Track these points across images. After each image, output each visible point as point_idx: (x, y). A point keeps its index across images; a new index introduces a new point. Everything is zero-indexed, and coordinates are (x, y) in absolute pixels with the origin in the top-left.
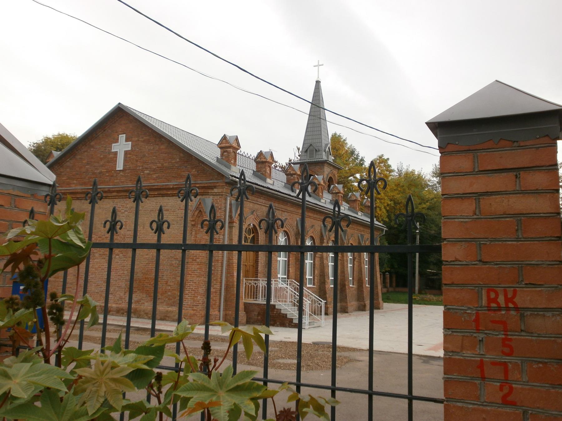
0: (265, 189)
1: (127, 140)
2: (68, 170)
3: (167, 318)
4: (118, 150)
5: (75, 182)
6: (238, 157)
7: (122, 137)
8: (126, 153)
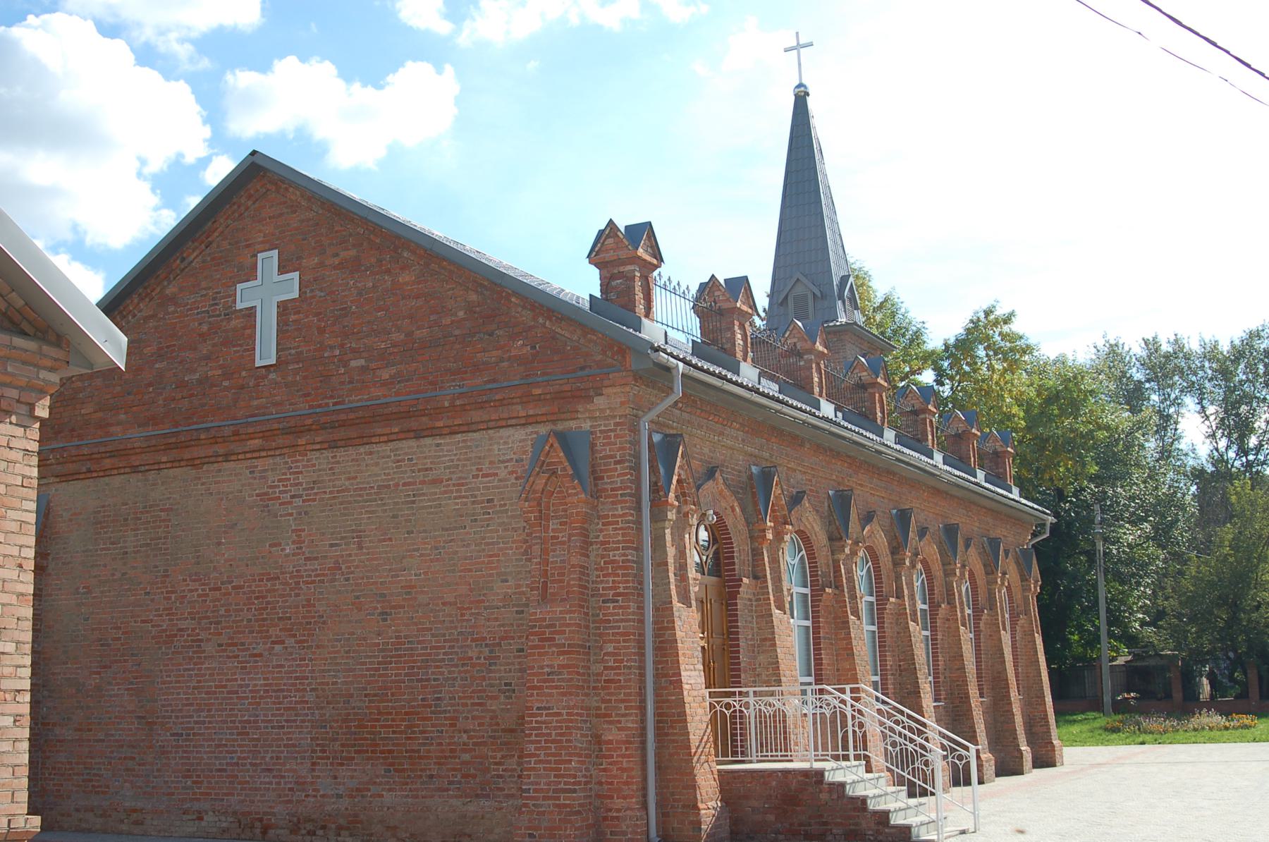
1: (283, 269)
4: (257, 303)
5: (123, 416)
6: (658, 296)
7: (269, 260)
8: (283, 307)
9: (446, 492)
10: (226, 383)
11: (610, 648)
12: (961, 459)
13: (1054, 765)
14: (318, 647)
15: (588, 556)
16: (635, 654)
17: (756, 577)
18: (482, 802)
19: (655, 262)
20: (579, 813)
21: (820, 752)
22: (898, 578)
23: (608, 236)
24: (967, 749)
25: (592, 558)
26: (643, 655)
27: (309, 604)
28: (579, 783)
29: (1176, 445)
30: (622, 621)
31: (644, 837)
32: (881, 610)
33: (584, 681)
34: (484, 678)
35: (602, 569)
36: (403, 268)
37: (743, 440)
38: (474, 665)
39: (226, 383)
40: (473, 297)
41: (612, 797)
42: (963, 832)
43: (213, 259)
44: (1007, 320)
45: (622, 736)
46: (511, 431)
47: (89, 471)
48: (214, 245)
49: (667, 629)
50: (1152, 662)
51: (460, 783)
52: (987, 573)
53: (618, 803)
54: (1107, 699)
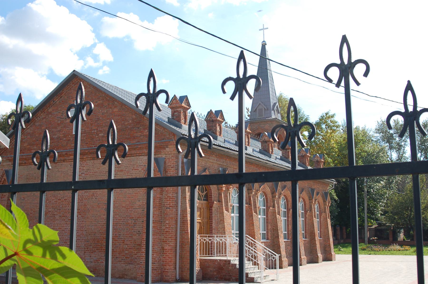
0: (256, 159)
2: (29, 136)
3: (125, 276)
9: (124, 174)
10: (64, 139)
11: (167, 222)
12: (303, 163)
13: (331, 260)
14: (87, 218)
15: (162, 195)
16: (174, 224)
17: (219, 201)
18: (131, 265)
19: (188, 107)
20: (156, 269)
21: (224, 254)
22: (274, 201)
23: (174, 100)
24: (275, 255)
25: (164, 194)
26: (177, 224)
27: (85, 205)
28: (156, 261)
29: (404, 155)
30: (171, 214)
31: (175, 277)
32: (267, 211)
33: (159, 231)
34: (132, 229)
35: (166, 199)
36: (115, 107)
37: (217, 160)
38: (130, 225)
39: (64, 139)
40: (134, 117)
41: (166, 266)
42: (273, 280)
43: (62, 102)
44: (332, 117)
45: (170, 248)
46: (143, 157)
47: (25, 163)
48: (63, 97)
49: (185, 217)
50: (383, 228)
51: (125, 259)
52: (309, 200)
53: (168, 267)
54: (366, 239)
